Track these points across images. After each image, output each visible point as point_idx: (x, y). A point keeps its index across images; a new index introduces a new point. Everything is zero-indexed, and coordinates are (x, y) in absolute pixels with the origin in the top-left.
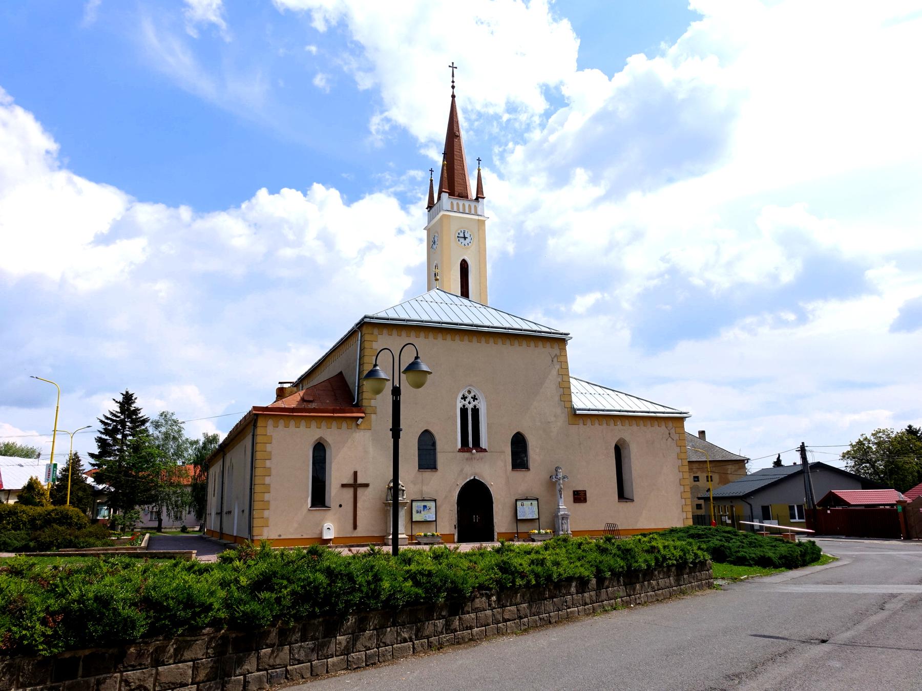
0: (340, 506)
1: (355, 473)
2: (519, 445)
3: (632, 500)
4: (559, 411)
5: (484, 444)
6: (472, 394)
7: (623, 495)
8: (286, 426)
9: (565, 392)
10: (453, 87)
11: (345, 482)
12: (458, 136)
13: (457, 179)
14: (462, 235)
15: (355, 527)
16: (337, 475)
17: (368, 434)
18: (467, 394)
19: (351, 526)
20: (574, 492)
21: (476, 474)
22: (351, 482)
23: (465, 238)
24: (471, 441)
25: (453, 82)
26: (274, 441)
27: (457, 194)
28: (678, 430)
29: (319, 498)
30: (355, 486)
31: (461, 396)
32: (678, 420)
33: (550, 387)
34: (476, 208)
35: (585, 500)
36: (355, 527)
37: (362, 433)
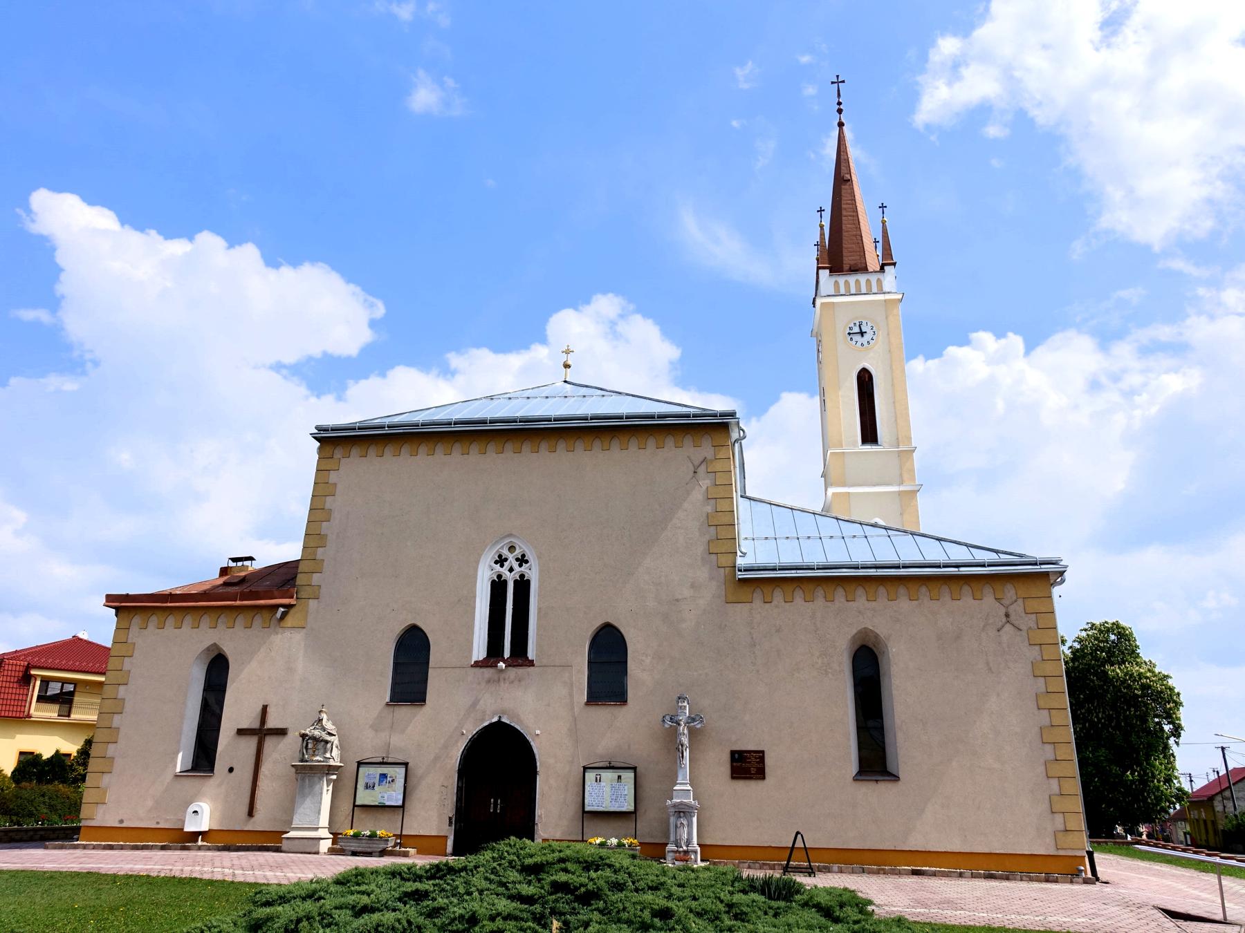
0: (231, 770)
1: (265, 708)
2: (608, 651)
4: (702, 574)
5: (531, 654)
6: (518, 553)
7: (875, 761)
8: (161, 627)
9: (721, 531)
10: (840, 111)
11: (245, 725)
12: (849, 181)
13: (847, 244)
14: (856, 330)
15: (251, 813)
16: (238, 711)
17: (298, 636)
18: (505, 553)
19: (245, 809)
20: (733, 753)
21: (504, 712)
22: (256, 725)
23: (862, 333)
24: (509, 641)
26: (136, 654)
27: (846, 267)
28: (1034, 605)
29: (204, 757)
30: (262, 733)
31: (529, 556)
32: (1035, 579)
33: (688, 522)
34: (879, 282)
35: (760, 774)
36: (251, 813)
37: (287, 634)
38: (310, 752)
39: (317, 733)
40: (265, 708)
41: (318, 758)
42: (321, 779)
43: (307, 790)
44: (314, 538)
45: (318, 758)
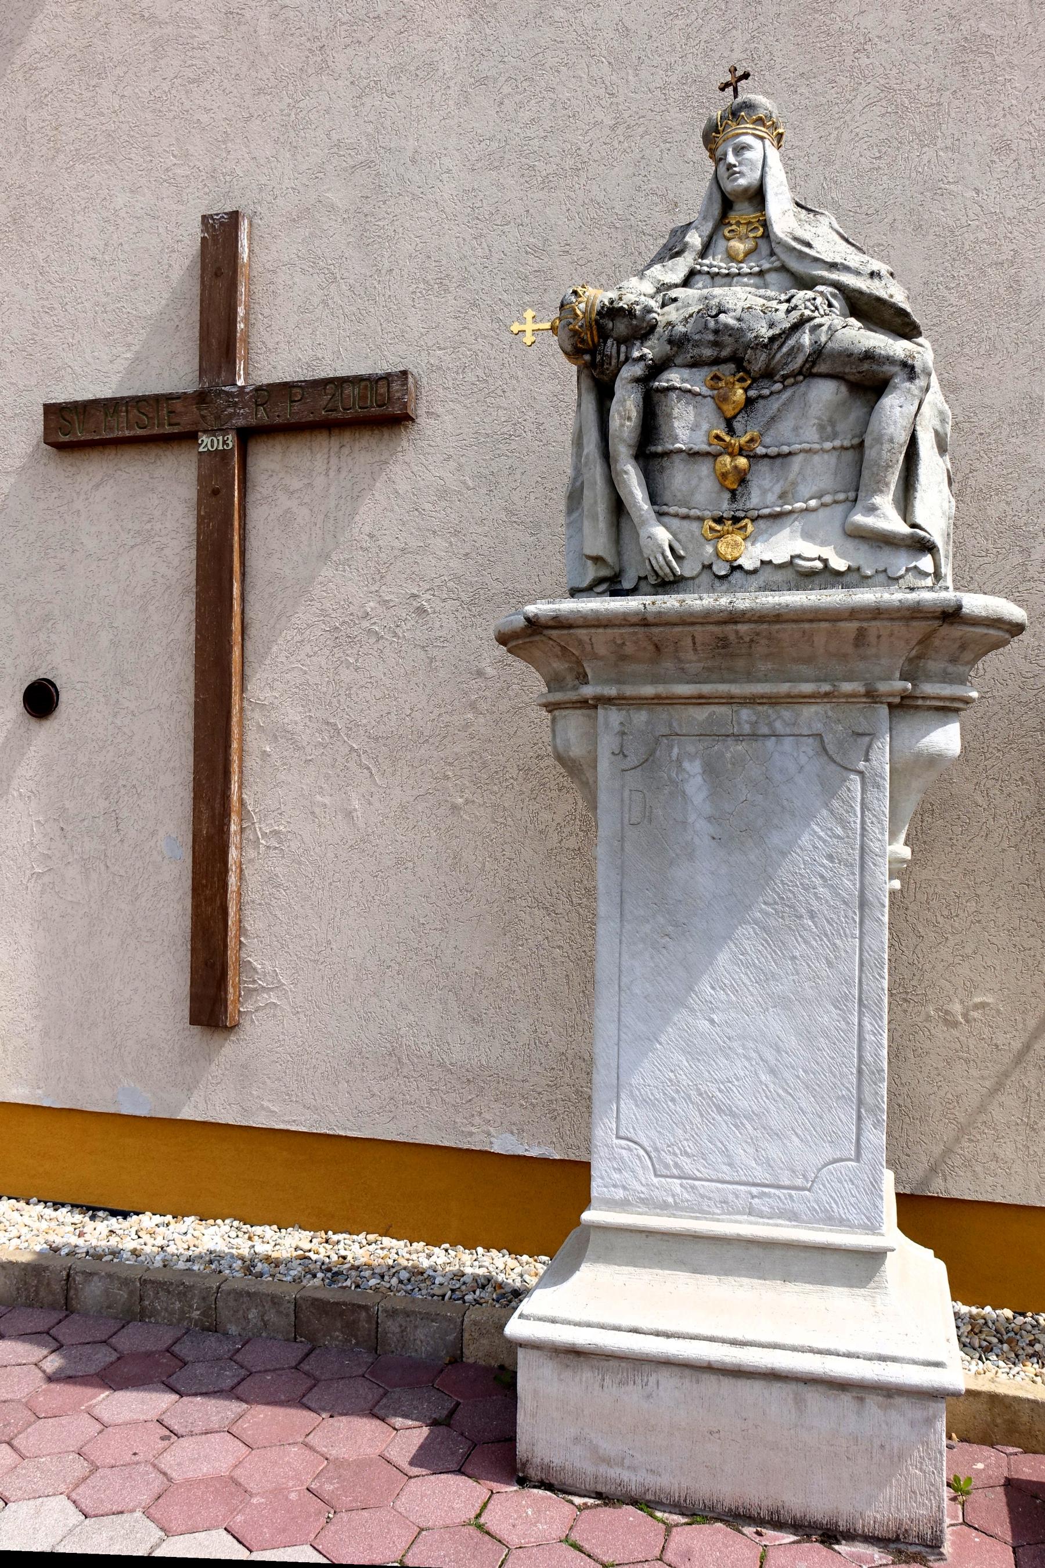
1: (221, 236)
15: (211, 1000)
19: (170, 976)
22: (175, 371)
36: (211, 1000)
38: (696, 485)
39: (749, 304)
40: (221, 236)
41: (784, 545)
42: (838, 758)
43: (703, 874)
44: (217, 1527)
45: (784, 545)
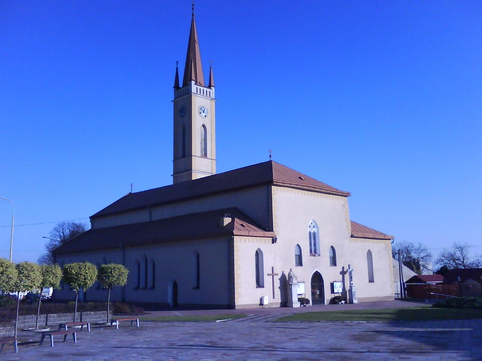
3: (263, 287)
10: (193, 9)
15: (258, 254)
16: (267, 270)
25: (193, 9)
